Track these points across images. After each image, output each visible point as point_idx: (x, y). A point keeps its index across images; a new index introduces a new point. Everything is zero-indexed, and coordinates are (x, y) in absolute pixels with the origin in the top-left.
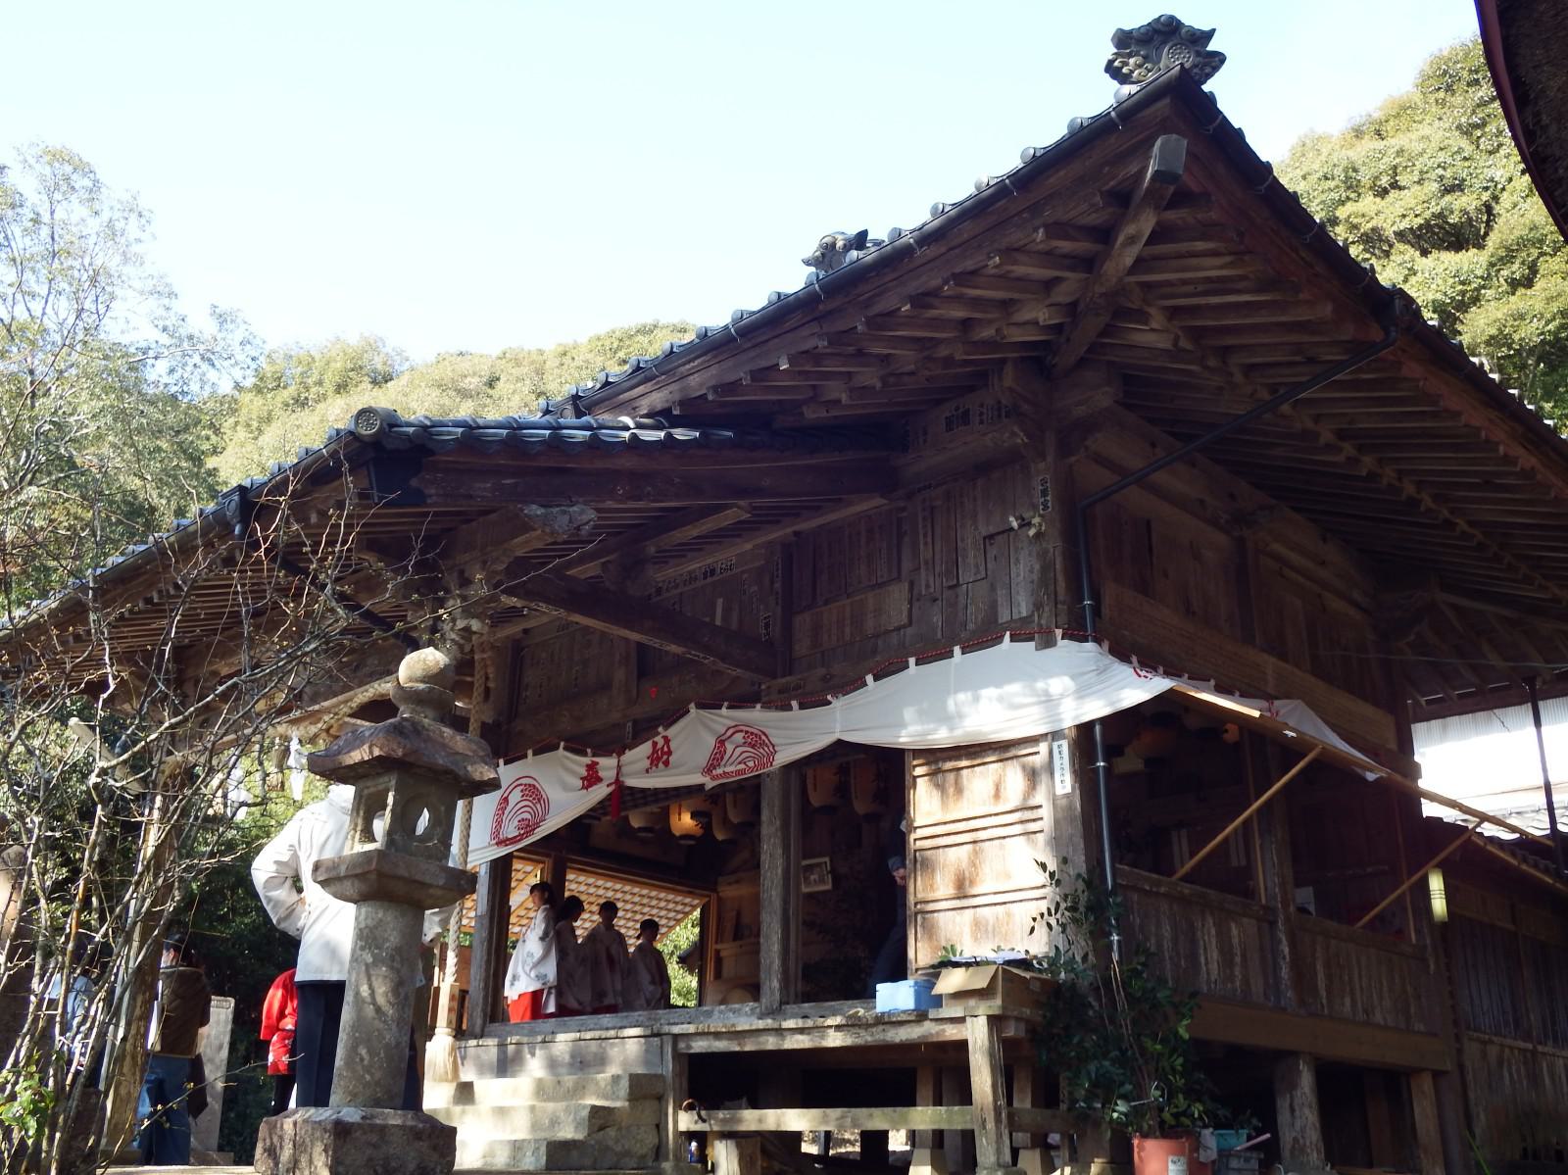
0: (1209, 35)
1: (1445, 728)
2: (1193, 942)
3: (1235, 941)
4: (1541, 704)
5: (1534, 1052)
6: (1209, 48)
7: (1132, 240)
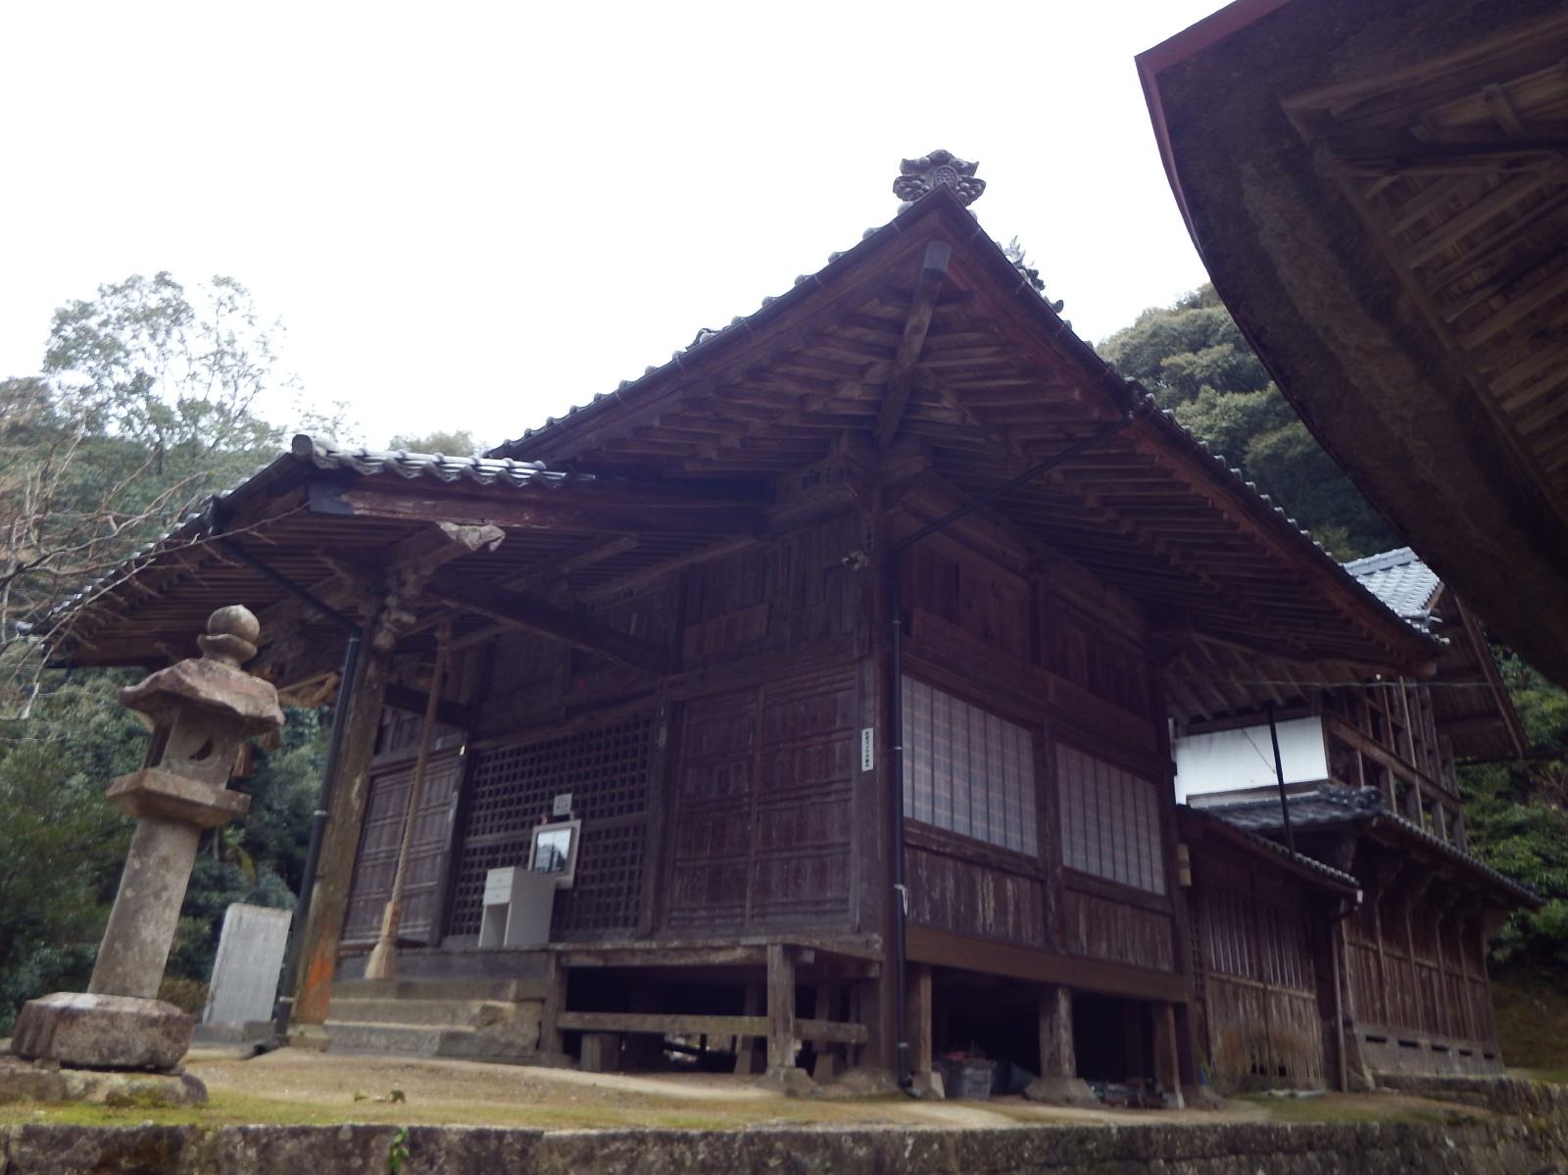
0: (973, 168)
1: (1211, 740)
2: (972, 893)
3: (1010, 894)
4: (1278, 726)
5: (1265, 991)
6: (975, 177)
7: (917, 330)
